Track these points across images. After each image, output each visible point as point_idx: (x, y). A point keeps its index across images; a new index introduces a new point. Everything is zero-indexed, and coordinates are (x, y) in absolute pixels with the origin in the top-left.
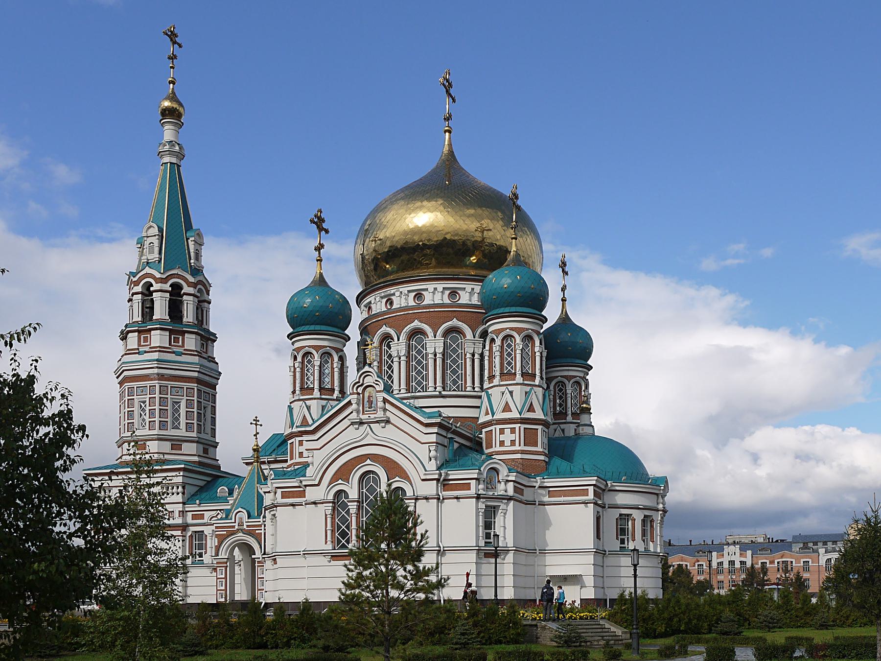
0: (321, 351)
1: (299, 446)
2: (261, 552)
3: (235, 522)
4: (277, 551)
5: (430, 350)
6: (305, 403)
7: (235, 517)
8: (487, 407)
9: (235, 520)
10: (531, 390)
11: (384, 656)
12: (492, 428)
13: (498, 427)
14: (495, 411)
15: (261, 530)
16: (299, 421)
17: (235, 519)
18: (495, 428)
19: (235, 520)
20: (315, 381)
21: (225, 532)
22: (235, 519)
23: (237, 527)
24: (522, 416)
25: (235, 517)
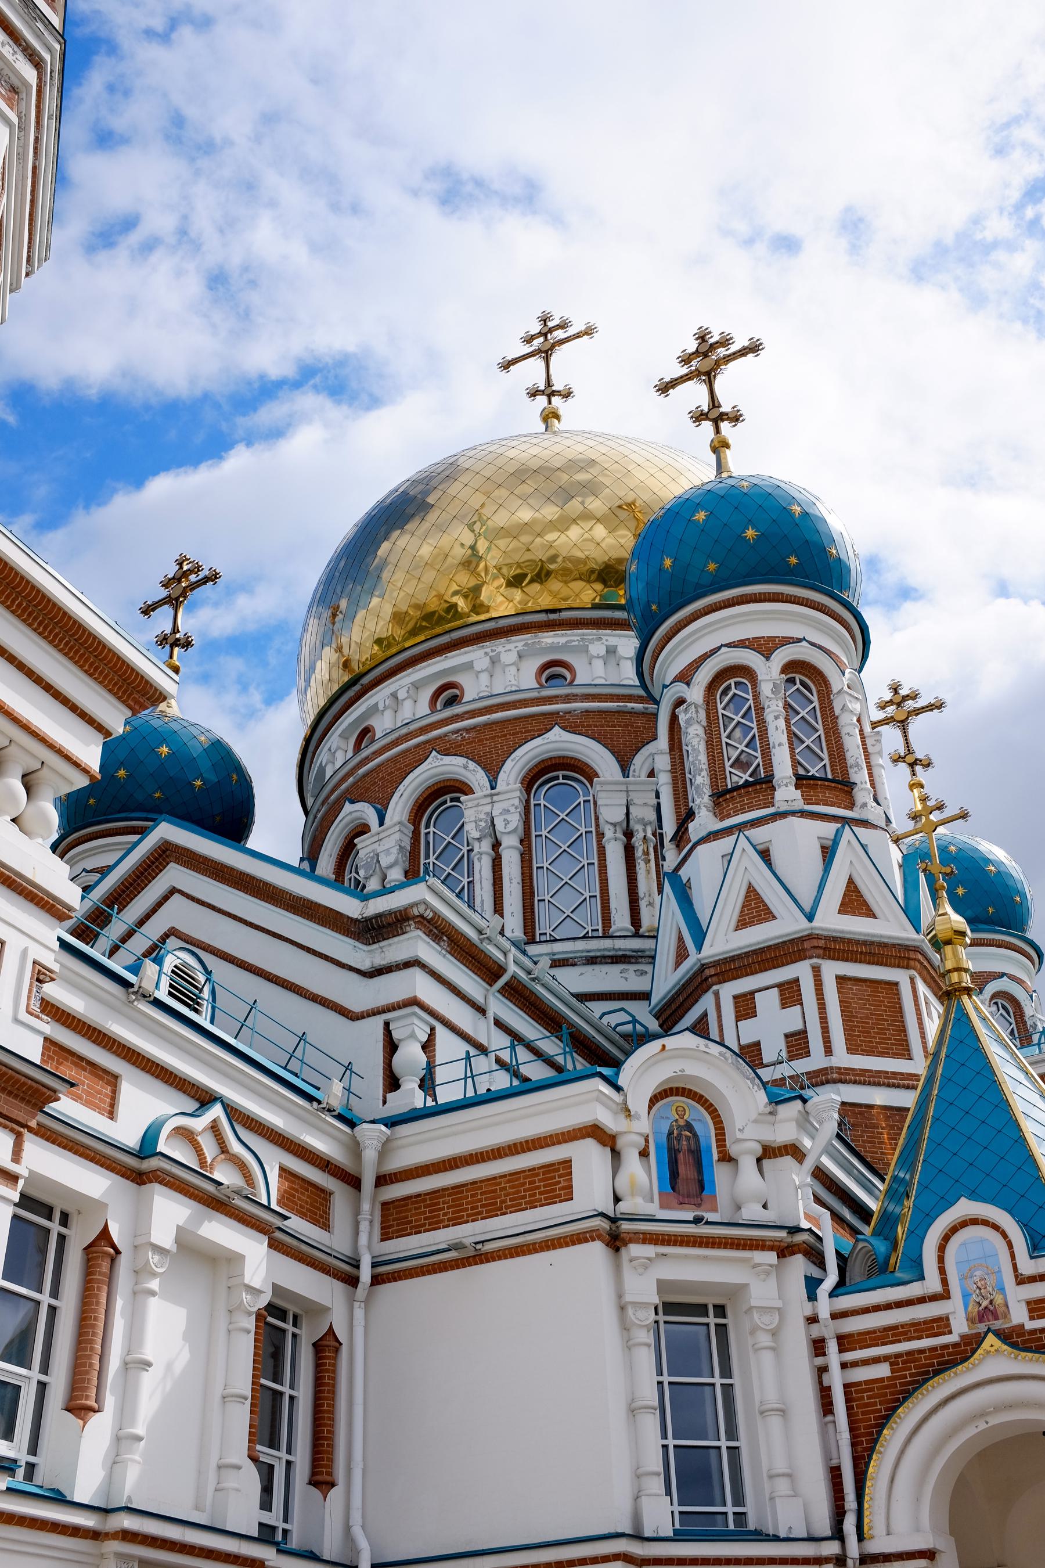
0: (782, 656)
1: (779, 985)
2: (1033, 964)
3: (945, 1295)
4: (656, 1403)
5: (612, 813)
7: (941, 1260)
8: (681, 939)
9: (944, 1282)
10: (838, 834)
11: (820, 1174)
12: (843, 1058)
13: (729, 990)
14: (586, 1003)
15: (828, 1051)
16: (340, 825)
17: (942, 1271)
18: (816, 971)
19: (944, 1282)
20: (483, 881)
21: (883, 1371)
22: (942, 1271)
23: (960, 1327)
25: (941, 1260)
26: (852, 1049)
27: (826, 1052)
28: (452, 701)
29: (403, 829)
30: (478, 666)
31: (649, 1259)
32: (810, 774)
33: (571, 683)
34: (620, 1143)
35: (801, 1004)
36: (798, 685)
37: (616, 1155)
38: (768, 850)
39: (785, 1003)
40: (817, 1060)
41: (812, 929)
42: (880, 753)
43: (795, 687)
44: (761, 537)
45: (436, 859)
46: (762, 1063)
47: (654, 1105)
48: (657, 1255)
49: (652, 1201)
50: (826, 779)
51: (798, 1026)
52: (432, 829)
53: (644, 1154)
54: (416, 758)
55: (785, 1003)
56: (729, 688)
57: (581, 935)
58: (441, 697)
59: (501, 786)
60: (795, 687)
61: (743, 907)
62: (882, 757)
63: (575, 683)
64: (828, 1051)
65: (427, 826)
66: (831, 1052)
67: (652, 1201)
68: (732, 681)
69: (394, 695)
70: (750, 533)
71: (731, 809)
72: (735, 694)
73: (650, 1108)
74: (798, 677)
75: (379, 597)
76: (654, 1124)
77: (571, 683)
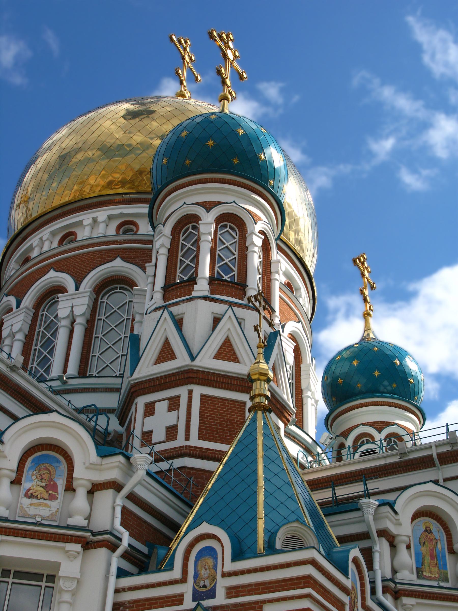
6: (171, 314)
15: (187, 438)
18: (190, 392)
24: (196, 363)
26: (201, 437)
27: (186, 438)
28: (74, 240)
29: (28, 311)
30: (85, 223)
31: (413, 605)
32: (224, 279)
33: (136, 233)
34: (397, 540)
35: (178, 410)
36: (228, 229)
37: (393, 546)
38: (182, 320)
39: (170, 409)
40: (180, 442)
41: (192, 366)
42: (278, 272)
43: (226, 230)
44: (216, 145)
45: (44, 329)
46: (151, 443)
47: (415, 519)
48: (417, 603)
49: (413, 574)
50: (234, 283)
51: (174, 422)
52: (45, 312)
53: (408, 547)
54: (43, 272)
55: (170, 409)
56: (188, 229)
57: (114, 375)
58: (66, 240)
59: (82, 289)
60: (226, 230)
61: (161, 352)
62: (279, 274)
63: (138, 233)
64: (187, 438)
65: (43, 311)
66: (189, 438)
67: (413, 574)
68: (190, 225)
69: (41, 239)
70: (211, 143)
71: (84, 275)
72: (191, 232)
73: (411, 522)
74: (229, 224)
75: (68, 190)
76: (413, 530)
77: (136, 233)
